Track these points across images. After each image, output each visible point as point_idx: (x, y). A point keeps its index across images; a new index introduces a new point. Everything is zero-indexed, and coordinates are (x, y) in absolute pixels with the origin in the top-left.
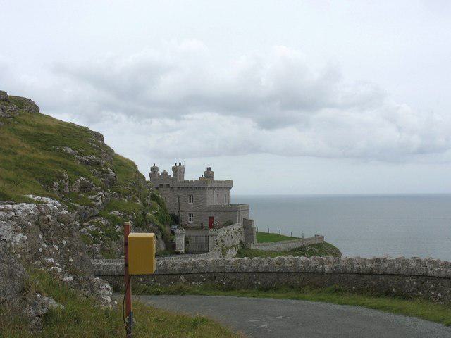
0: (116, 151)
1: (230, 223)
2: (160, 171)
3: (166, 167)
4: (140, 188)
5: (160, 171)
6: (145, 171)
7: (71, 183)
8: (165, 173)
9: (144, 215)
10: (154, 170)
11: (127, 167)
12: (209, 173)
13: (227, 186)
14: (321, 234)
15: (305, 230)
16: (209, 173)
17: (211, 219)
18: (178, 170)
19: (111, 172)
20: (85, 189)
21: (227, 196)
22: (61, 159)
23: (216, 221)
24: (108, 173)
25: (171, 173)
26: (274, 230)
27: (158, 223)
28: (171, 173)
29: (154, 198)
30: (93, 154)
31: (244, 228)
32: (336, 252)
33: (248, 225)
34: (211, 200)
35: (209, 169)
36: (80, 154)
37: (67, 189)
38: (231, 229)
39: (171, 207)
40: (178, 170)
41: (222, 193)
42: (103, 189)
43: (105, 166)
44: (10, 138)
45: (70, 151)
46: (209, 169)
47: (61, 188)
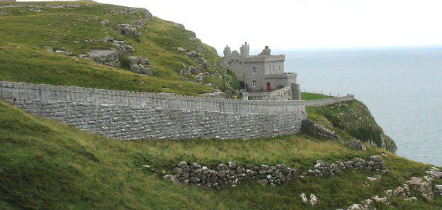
0: (202, 42)
1: (281, 87)
2: (232, 50)
3: (235, 47)
4: (220, 67)
5: (232, 50)
6: (221, 53)
7: (187, 70)
8: (235, 52)
9: (224, 85)
10: (227, 50)
11: (210, 52)
12: (266, 51)
13: (281, 59)
14: (351, 93)
15: (334, 86)
16: (266, 51)
17: (269, 84)
18: (245, 48)
19: (205, 60)
20: (193, 72)
21: (281, 68)
22: (179, 56)
23: (272, 85)
24: (202, 61)
25: (239, 52)
26: (317, 91)
27: (232, 89)
28: (239, 52)
29: (229, 72)
30: (194, 50)
31: (292, 90)
32: (391, 146)
33: (295, 88)
34: (268, 70)
35: (267, 47)
36: (187, 51)
37: (186, 73)
38: (282, 91)
39: (239, 76)
40: (245, 48)
41: (277, 65)
42: (202, 71)
43: (201, 56)
44: (186, 200)
45: (182, 49)
46: (267, 47)
47: (184, 72)
